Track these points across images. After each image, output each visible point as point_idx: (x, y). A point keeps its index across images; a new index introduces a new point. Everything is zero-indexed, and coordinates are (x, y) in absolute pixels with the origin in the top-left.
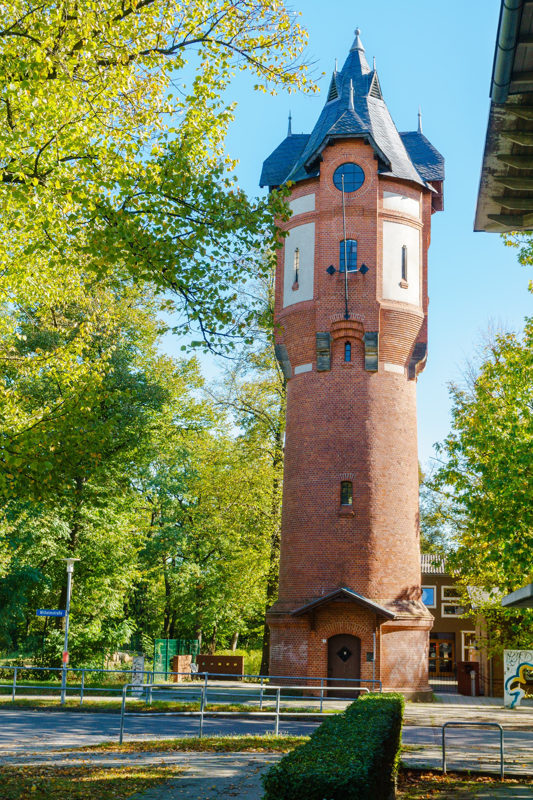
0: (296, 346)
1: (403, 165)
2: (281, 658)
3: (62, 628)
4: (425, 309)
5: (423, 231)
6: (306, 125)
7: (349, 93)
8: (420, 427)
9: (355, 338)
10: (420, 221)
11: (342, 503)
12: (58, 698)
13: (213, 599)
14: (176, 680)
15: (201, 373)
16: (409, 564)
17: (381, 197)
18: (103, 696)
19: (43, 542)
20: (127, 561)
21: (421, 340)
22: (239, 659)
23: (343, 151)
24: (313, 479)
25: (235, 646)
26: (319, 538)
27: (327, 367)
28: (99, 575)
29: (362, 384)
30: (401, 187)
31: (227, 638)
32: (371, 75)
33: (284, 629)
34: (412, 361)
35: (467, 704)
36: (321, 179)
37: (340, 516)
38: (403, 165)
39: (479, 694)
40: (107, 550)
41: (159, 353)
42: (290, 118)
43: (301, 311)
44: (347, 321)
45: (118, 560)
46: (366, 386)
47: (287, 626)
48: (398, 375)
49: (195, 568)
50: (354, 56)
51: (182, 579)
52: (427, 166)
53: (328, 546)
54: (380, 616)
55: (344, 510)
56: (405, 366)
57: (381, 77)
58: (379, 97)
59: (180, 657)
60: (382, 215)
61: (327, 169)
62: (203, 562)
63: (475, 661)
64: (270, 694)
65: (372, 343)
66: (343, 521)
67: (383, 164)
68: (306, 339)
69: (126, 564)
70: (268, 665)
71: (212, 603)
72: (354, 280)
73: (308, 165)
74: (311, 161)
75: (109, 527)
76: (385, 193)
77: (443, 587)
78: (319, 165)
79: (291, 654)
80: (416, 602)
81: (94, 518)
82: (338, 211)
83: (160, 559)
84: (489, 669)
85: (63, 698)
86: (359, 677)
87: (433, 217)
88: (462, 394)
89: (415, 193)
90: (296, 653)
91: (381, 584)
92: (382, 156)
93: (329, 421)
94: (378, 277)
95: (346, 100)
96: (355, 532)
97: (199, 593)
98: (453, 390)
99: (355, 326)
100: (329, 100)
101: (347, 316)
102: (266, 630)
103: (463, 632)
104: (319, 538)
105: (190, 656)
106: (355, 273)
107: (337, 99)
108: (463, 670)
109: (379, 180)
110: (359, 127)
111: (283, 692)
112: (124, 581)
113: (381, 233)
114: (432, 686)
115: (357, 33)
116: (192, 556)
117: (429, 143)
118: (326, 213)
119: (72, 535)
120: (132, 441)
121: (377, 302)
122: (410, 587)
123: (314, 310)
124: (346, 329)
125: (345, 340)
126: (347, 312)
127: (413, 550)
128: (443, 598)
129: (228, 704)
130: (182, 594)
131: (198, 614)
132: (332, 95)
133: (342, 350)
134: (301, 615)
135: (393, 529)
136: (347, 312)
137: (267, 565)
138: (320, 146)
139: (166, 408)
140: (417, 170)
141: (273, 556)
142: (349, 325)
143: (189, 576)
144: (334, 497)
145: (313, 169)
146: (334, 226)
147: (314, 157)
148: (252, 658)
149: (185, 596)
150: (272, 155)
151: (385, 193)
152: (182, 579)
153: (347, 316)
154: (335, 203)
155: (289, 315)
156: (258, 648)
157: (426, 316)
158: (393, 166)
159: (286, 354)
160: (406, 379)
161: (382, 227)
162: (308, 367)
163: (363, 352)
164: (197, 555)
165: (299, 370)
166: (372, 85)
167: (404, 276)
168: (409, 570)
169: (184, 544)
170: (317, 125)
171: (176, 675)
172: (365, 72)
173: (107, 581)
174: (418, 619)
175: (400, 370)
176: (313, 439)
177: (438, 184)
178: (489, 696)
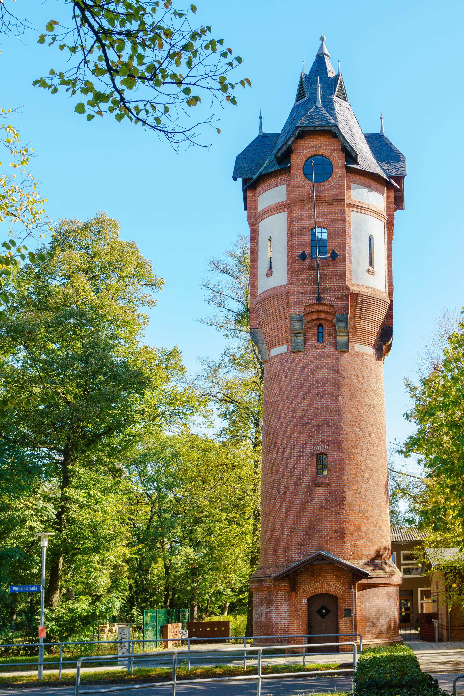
0: (272, 329)
1: (367, 160)
2: (264, 619)
3: (52, 605)
4: (390, 294)
5: (388, 224)
6: (276, 125)
7: (316, 93)
8: (389, 399)
9: (327, 320)
10: (385, 213)
11: (318, 473)
12: (36, 673)
13: (205, 576)
14: (166, 646)
15: (182, 363)
16: (380, 527)
17: (349, 188)
18: (88, 667)
19: (28, 523)
20: (113, 538)
21: (388, 324)
22: (226, 624)
23: (312, 144)
24: (290, 452)
25: (226, 613)
26: (297, 507)
27: (301, 347)
28: (86, 552)
29: (334, 363)
30: (367, 181)
31: (219, 607)
32: (337, 77)
33: (265, 592)
34: (379, 343)
35: (434, 649)
36: (292, 170)
37: (316, 485)
38: (367, 160)
39: (440, 640)
40: (95, 528)
41: (140, 345)
42: (261, 118)
43: (274, 296)
44: (319, 304)
45: (104, 538)
46: (338, 365)
47: (269, 589)
48: (368, 355)
49: (189, 550)
50: (320, 60)
51: (178, 561)
52: (390, 163)
53: (306, 513)
54: (355, 576)
55: (320, 480)
56: (374, 347)
57: (348, 81)
58: (345, 98)
59: (170, 626)
60: (350, 205)
61: (297, 161)
62: (196, 545)
63: (431, 611)
64: (253, 654)
65: (343, 324)
66: (319, 490)
67: (350, 156)
68: (281, 322)
69: (113, 541)
70: (252, 627)
71: (204, 580)
72: (324, 266)
73: (279, 155)
74: (282, 152)
75: (96, 507)
76: (352, 185)
77: (402, 553)
78: (289, 157)
79: (273, 615)
80: (387, 561)
81: (81, 499)
82: (309, 200)
83: (158, 545)
84: (447, 618)
85: (40, 673)
86: (337, 632)
87: (396, 213)
88: (415, 388)
89: (379, 187)
90: (278, 614)
91: (355, 546)
92: (348, 148)
93: (304, 398)
94: (347, 263)
95: (313, 99)
96: (330, 499)
97: (194, 571)
98: (408, 385)
99: (326, 308)
100: (297, 100)
101: (319, 299)
102: (251, 596)
103: (419, 589)
104: (297, 507)
105: (180, 624)
106: (326, 259)
107: (305, 99)
108: (424, 620)
109: (347, 172)
110: (327, 120)
111: (265, 652)
112: (112, 558)
113: (350, 223)
114: (402, 635)
115: (322, 39)
116: (186, 541)
117: (391, 144)
118: (297, 202)
119: (59, 516)
120: (117, 427)
121: (347, 286)
122: (382, 548)
123: (288, 294)
124: (318, 312)
125: (317, 323)
126: (319, 295)
127: (383, 514)
128: (402, 562)
129: (213, 665)
130: (179, 573)
131: (193, 589)
132: (300, 95)
133: (315, 331)
134: (282, 579)
135: (366, 496)
136: (319, 295)
137: (249, 539)
138: (290, 137)
139: (147, 392)
140: (381, 167)
141: (255, 530)
142: (321, 308)
143: (184, 558)
144: (310, 468)
145: (284, 158)
146: (305, 214)
147: (285, 148)
148: (238, 622)
149: (181, 575)
150: (245, 151)
151: (352, 185)
152: (178, 561)
153: (319, 299)
154: (305, 192)
155: (264, 300)
156: (244, 613)
157: (391, 302)
158: (360, 160)
159: (261, 338)
160: (374, 359)
161: (350, 216)
162: (283, 349)
163: (335, 333)
164: (191, 540)
165: (274, 352)
166: (337, 87)
167: (371, 264)
168: (381, 533)
169: (179, 531)
170: (286, 123)
171: (167, 642)
172: (331, 75)
173: (97, 558)
174: (391, 576)
175: (369, 350)
176: (290, 415)
177: (399, 179)
178: (448, 641)
